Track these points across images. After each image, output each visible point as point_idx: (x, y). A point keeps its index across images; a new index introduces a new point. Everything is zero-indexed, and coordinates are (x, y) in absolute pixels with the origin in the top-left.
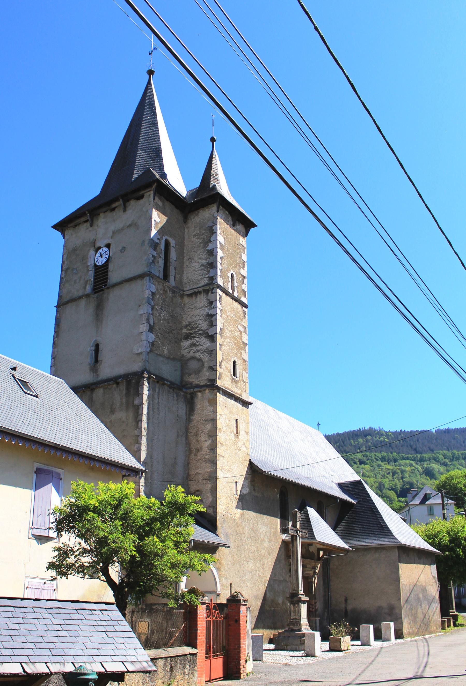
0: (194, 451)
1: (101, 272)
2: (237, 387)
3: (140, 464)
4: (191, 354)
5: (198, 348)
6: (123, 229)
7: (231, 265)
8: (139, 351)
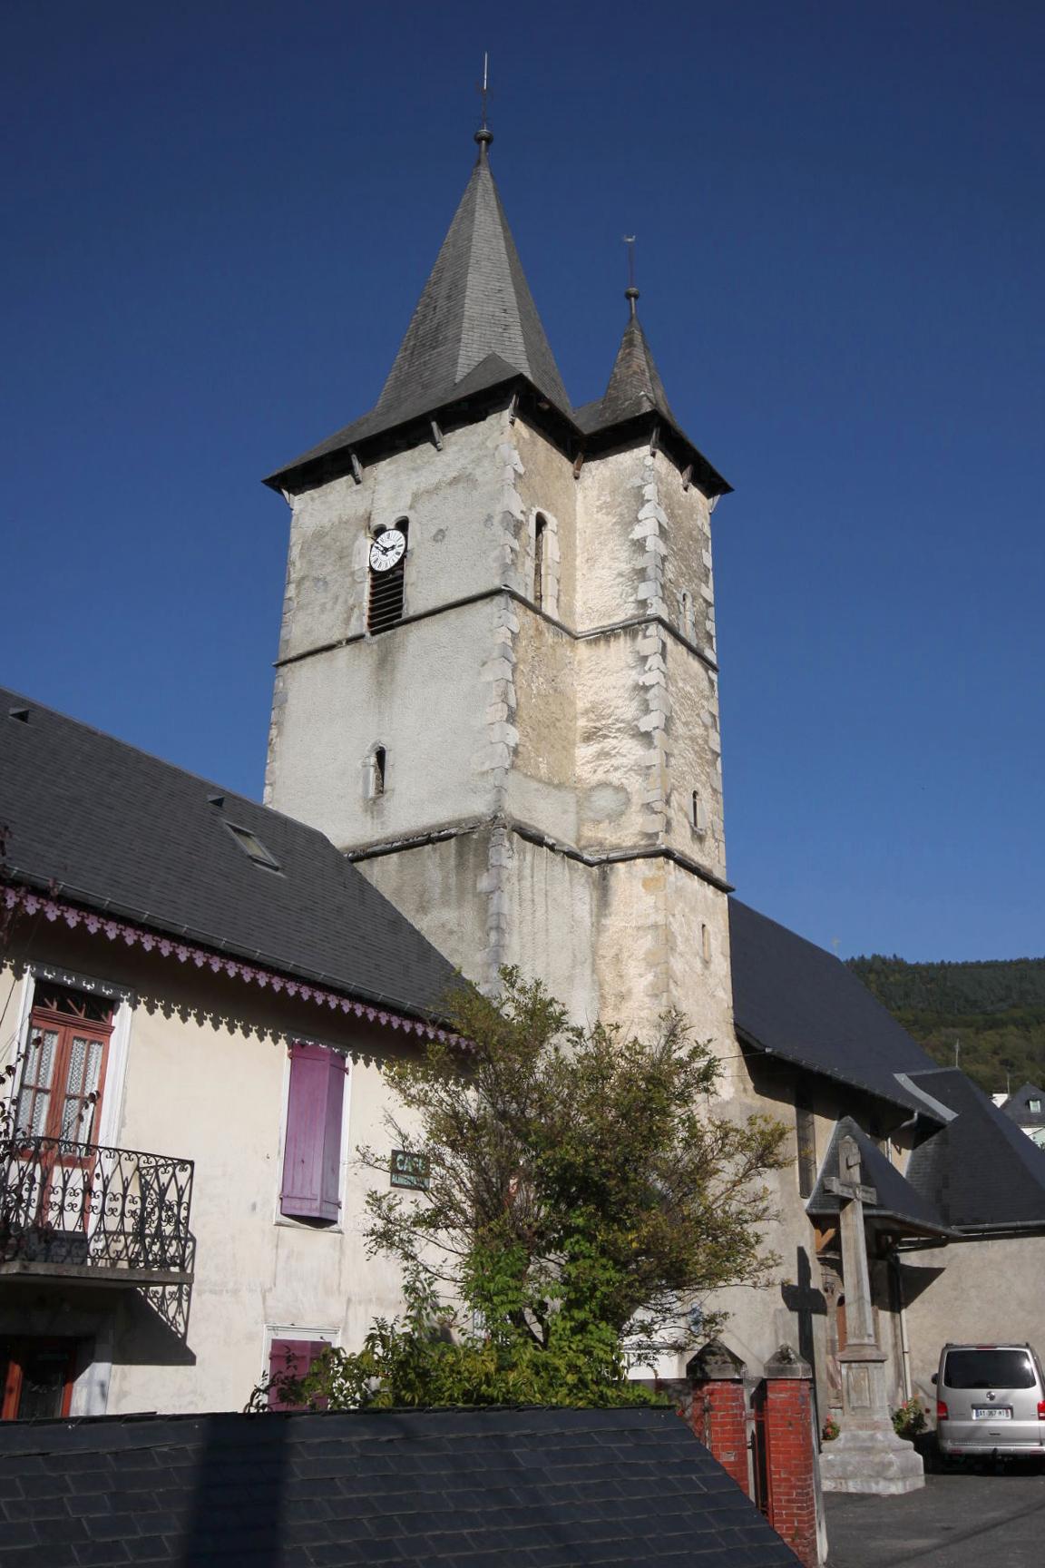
0: (611, 1000)
1: (388, 588)
2: (702, 850)
3: (838, 1234)
4: (600, 776)
5: (615, 762)
6: (437, 488)
7: (682, 575)
8: (485, 768)
